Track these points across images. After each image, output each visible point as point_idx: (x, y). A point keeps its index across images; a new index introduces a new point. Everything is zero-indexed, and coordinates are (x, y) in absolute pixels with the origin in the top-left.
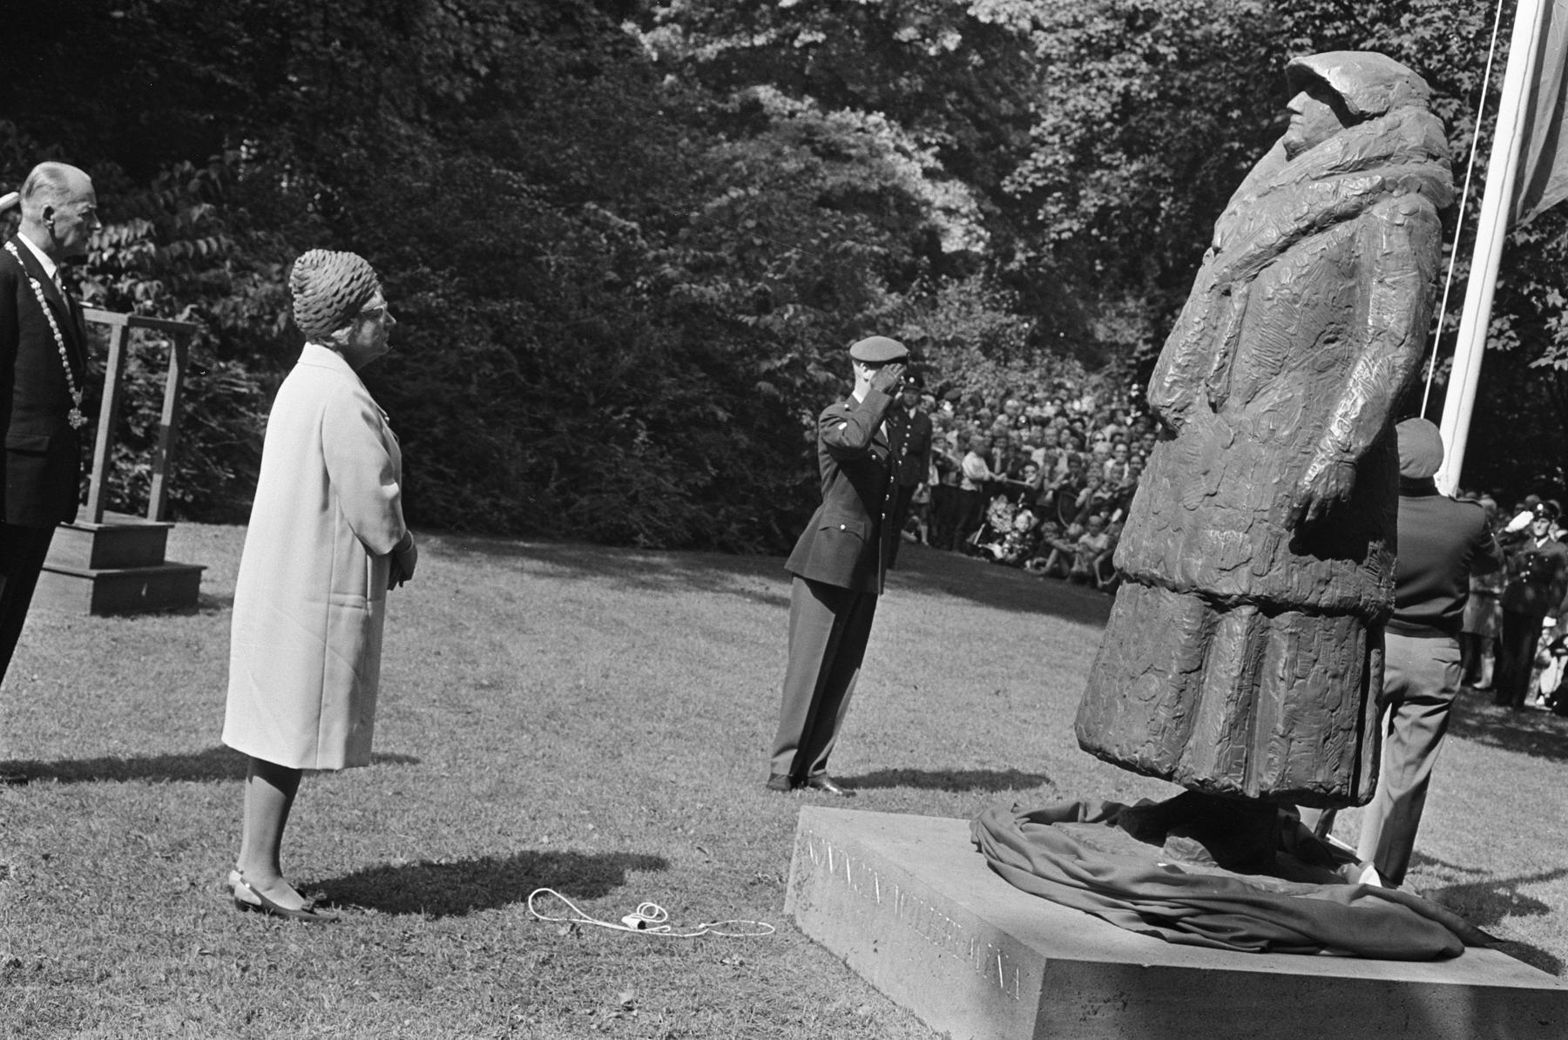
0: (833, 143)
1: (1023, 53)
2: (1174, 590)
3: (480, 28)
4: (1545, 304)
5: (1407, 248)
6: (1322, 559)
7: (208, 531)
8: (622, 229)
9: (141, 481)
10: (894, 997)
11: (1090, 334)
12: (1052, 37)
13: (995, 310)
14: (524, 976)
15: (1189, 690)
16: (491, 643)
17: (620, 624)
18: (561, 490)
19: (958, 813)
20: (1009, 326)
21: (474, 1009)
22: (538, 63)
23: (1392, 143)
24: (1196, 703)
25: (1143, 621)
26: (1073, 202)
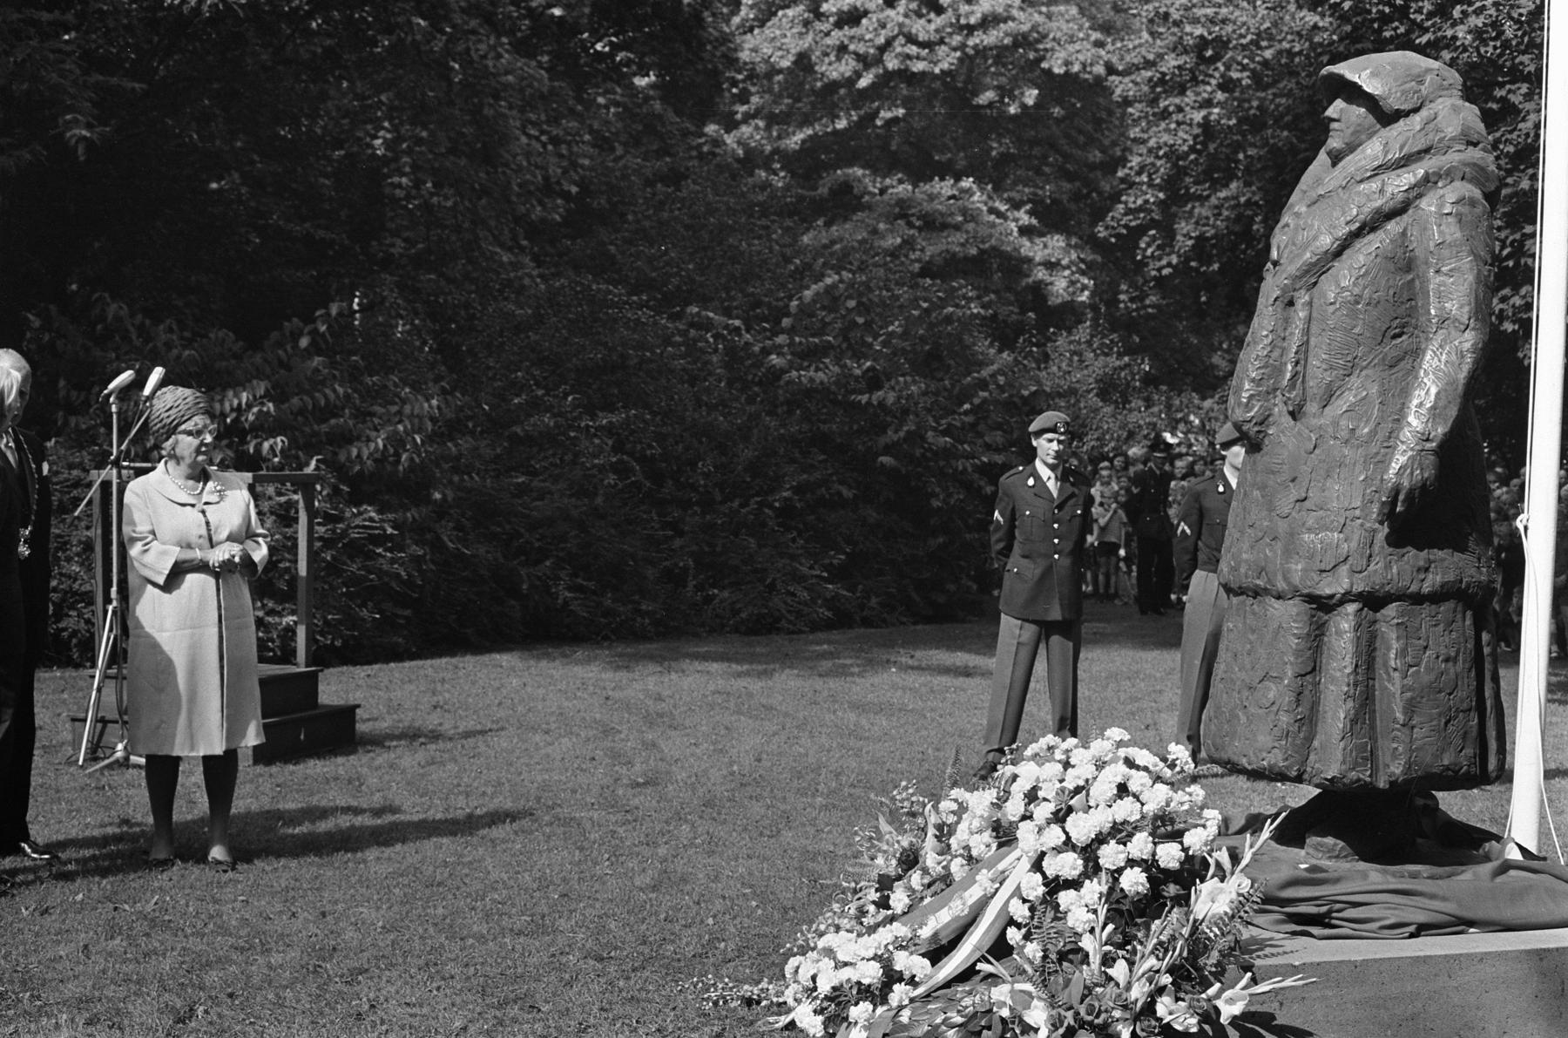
2: (1279, 597)
3: (564, 150)
5: (1458, 235)
7: (361, 672)
9: (290, 632)
12: (1127, 80)
13: (1107, 355)
15: (1307, 692)
16: (643, 743)
17: (769, 708)
18: (699, 588)
20: (1122, 368)
22: (624, 177)
23: (1431, 136)
24: (1315, 706)
25: (1253, 631)
26: (1169, 235)
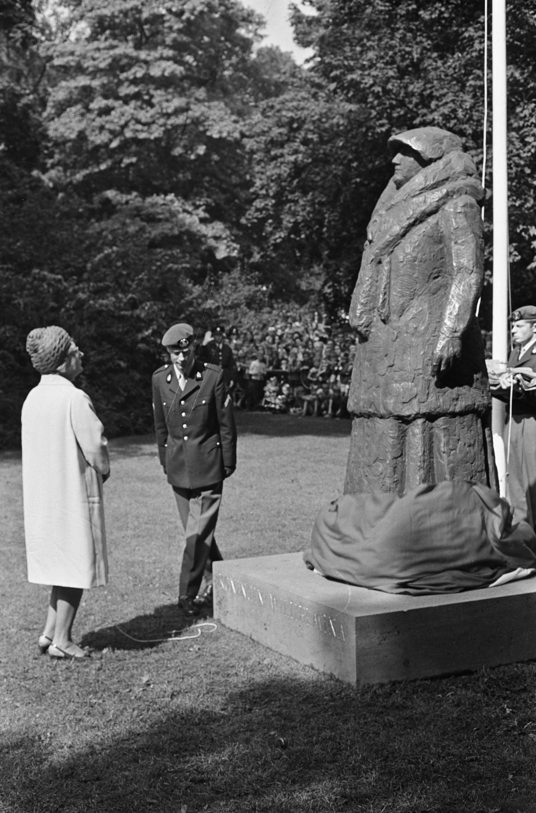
0: (151, 214)
1: (238, 151)
2: (382, 417)
4: (529, 235)
5: (465, 223)
6: (452, 387)
8: (54, 279)
10: (280, 650)
11: (298, 288)
12: (252, 140)
13: (249, 284)
14: (91, 679)
19: (289, 548)
21: (70, 702)
24: (403, 474)
25: (369, 436)
